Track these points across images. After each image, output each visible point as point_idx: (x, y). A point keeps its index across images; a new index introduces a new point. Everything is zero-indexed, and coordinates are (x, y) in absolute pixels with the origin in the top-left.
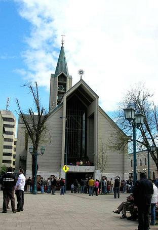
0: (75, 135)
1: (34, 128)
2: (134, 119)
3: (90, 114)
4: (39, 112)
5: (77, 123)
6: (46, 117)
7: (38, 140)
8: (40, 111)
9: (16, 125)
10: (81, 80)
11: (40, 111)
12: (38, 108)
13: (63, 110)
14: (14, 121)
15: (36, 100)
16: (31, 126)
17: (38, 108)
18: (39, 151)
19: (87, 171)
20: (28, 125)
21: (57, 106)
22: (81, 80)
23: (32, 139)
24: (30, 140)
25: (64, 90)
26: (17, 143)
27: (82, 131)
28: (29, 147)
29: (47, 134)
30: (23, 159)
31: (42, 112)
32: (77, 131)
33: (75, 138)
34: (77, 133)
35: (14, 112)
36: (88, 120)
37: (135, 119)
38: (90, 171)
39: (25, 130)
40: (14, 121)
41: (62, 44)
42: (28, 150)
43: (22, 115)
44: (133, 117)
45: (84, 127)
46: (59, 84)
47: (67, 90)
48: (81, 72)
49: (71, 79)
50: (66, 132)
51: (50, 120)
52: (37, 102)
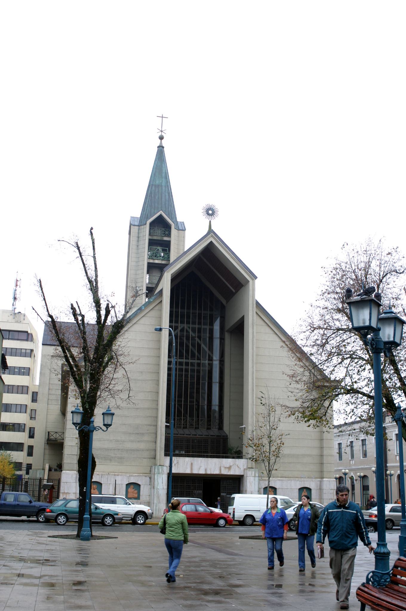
0: (193, 377)
1: (86, 359)
2: (376, 331)
3: (232, 322)
4: (98, 312)
5: (199, 346)
6: (119, 326)
7: (95, 389)
8: (103, 313)
9: (39, 350)
10: (211, 231)
11: (103, 313)
12: (97, 303)
13: (161, 310)
14: (32, 340)
15: (90, 282)
16: (75, 351)
17: (97, 303)
18: (98, 420)
19: (225, 472)
20: (69, 351)
21: (144, 300)
22: (211, 231)
23: (79, 384)
24: (73, 388)
25: (164, 258)
26: (39, 397)
27: (211, 365)
28: (70, 408)
29: (120, 373)
30: (56, 440)
31: (108, 312)
32: (199, 364)
33: (192, 393)
34: (198, 371)
35: (31, 317)
36: (227, 336)
37: (379, 330)
38: (232, 473)
39: (61, 362)
40: (32, 340)
41: (161, 138)
42: (69, 416)
43: (53, 321)
44: (374, 325)
45: (216, 357)
46: (152, 243)
47: (172, 260)
48: (210, 212)
49: (182, 229)
50: (169, 369)
51: (127, 335)
52: (94, 289)
